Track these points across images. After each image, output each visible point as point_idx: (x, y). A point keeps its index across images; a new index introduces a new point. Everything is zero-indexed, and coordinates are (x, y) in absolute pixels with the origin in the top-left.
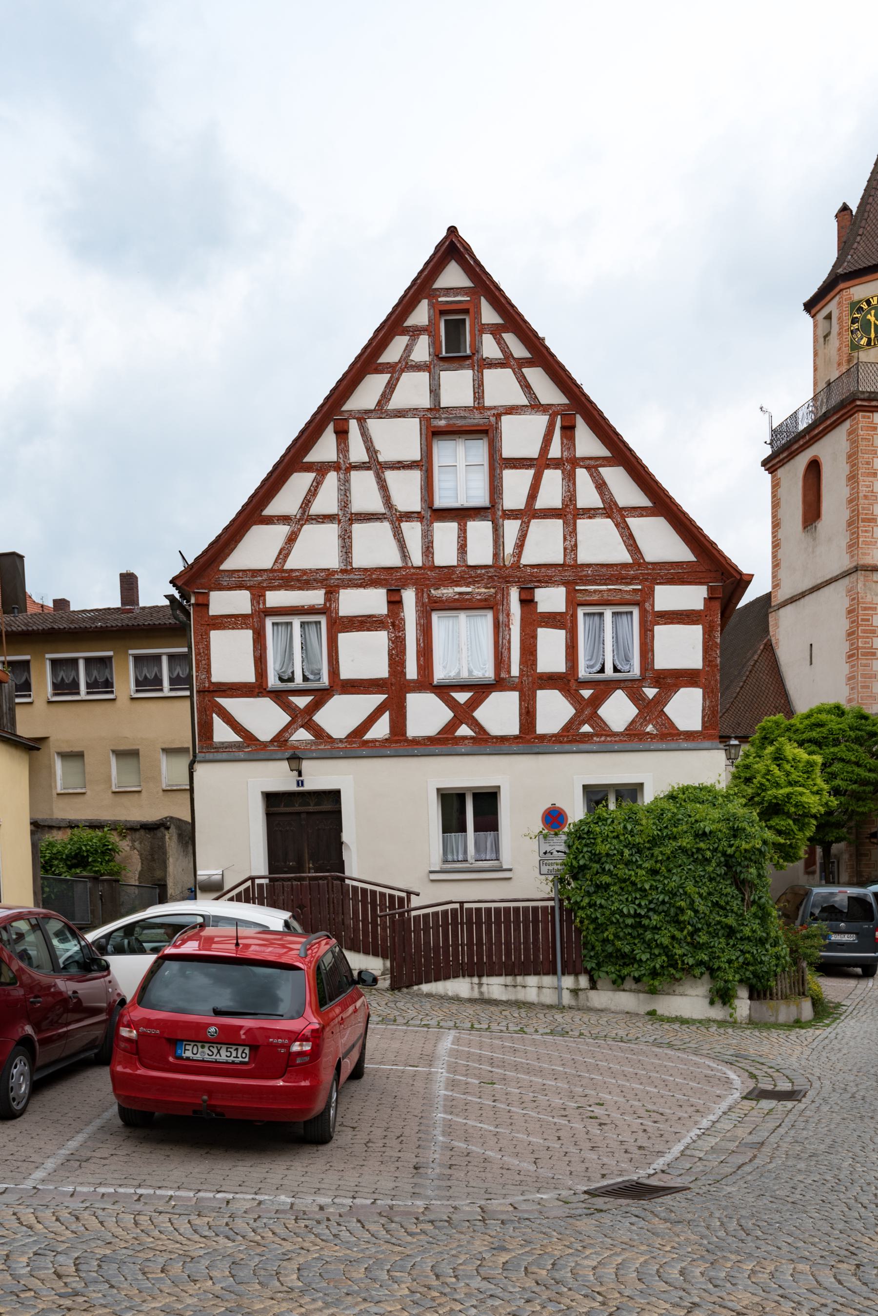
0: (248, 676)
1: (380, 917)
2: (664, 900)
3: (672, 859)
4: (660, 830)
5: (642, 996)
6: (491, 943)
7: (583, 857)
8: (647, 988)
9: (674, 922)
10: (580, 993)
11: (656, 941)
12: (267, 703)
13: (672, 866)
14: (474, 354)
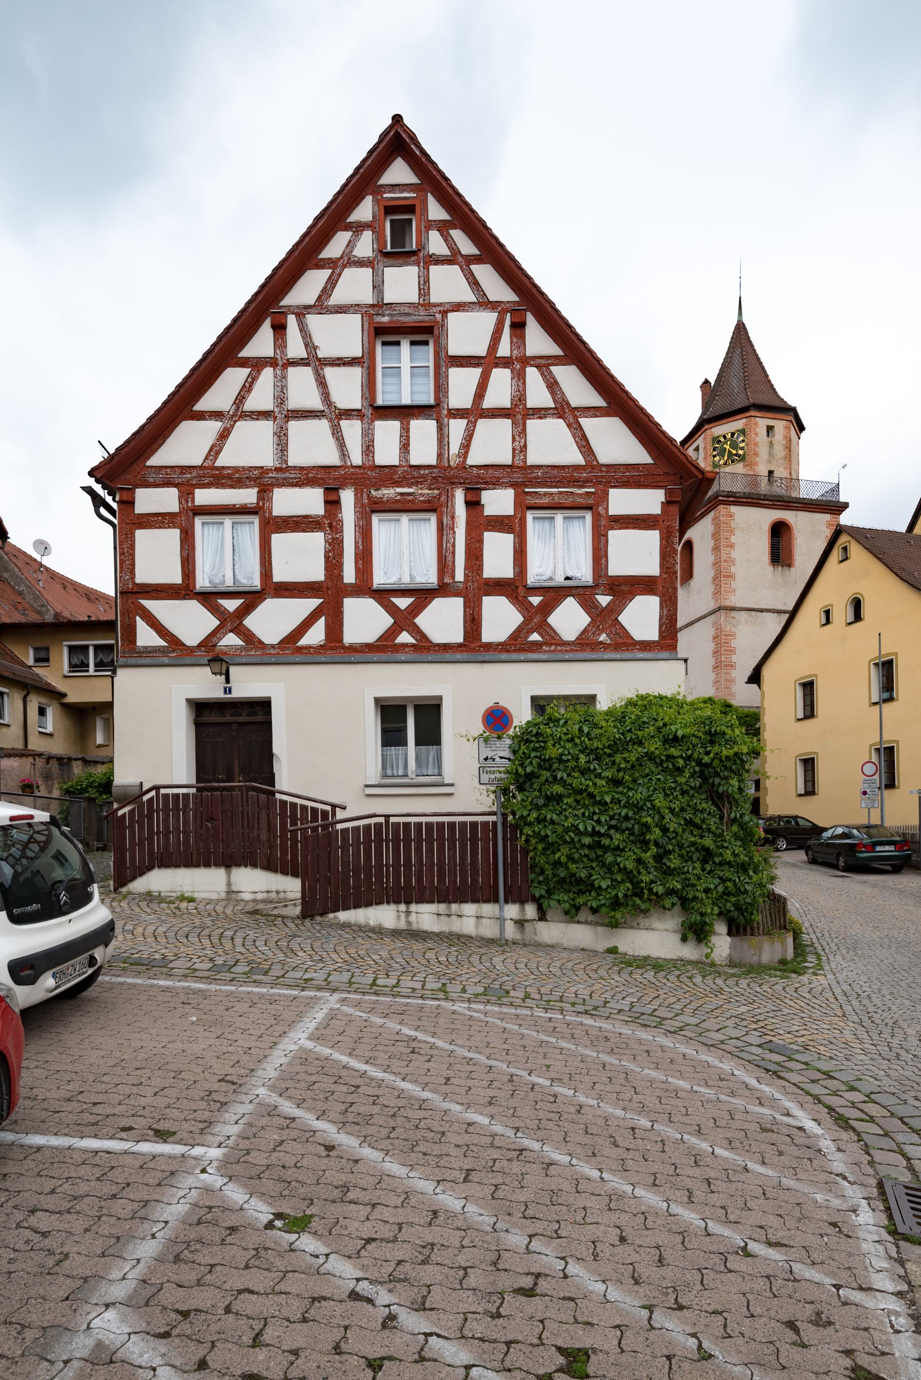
0: (176, 577)
1: (290, 831)
2: (627, 815)
3: (637, 767)
4: (622, 734)
5: (600, 929)
6: (421, 865)
7: (531, 763)
8: (607, 921)
9: (640, 842)
10: (526, 924)
11: (618, 864)
12: (193, 607)
13: (637, 775)
14: (420, 250)
